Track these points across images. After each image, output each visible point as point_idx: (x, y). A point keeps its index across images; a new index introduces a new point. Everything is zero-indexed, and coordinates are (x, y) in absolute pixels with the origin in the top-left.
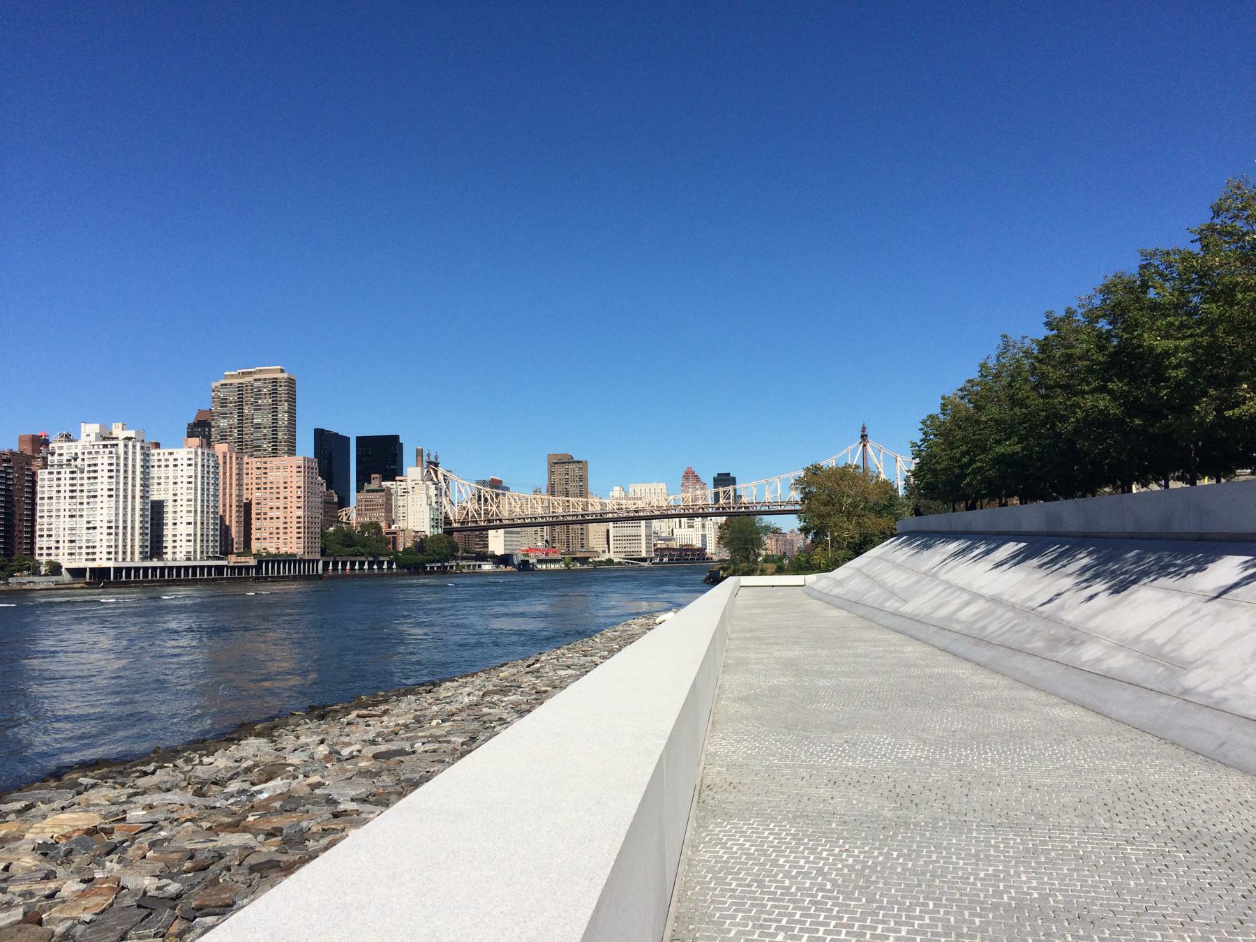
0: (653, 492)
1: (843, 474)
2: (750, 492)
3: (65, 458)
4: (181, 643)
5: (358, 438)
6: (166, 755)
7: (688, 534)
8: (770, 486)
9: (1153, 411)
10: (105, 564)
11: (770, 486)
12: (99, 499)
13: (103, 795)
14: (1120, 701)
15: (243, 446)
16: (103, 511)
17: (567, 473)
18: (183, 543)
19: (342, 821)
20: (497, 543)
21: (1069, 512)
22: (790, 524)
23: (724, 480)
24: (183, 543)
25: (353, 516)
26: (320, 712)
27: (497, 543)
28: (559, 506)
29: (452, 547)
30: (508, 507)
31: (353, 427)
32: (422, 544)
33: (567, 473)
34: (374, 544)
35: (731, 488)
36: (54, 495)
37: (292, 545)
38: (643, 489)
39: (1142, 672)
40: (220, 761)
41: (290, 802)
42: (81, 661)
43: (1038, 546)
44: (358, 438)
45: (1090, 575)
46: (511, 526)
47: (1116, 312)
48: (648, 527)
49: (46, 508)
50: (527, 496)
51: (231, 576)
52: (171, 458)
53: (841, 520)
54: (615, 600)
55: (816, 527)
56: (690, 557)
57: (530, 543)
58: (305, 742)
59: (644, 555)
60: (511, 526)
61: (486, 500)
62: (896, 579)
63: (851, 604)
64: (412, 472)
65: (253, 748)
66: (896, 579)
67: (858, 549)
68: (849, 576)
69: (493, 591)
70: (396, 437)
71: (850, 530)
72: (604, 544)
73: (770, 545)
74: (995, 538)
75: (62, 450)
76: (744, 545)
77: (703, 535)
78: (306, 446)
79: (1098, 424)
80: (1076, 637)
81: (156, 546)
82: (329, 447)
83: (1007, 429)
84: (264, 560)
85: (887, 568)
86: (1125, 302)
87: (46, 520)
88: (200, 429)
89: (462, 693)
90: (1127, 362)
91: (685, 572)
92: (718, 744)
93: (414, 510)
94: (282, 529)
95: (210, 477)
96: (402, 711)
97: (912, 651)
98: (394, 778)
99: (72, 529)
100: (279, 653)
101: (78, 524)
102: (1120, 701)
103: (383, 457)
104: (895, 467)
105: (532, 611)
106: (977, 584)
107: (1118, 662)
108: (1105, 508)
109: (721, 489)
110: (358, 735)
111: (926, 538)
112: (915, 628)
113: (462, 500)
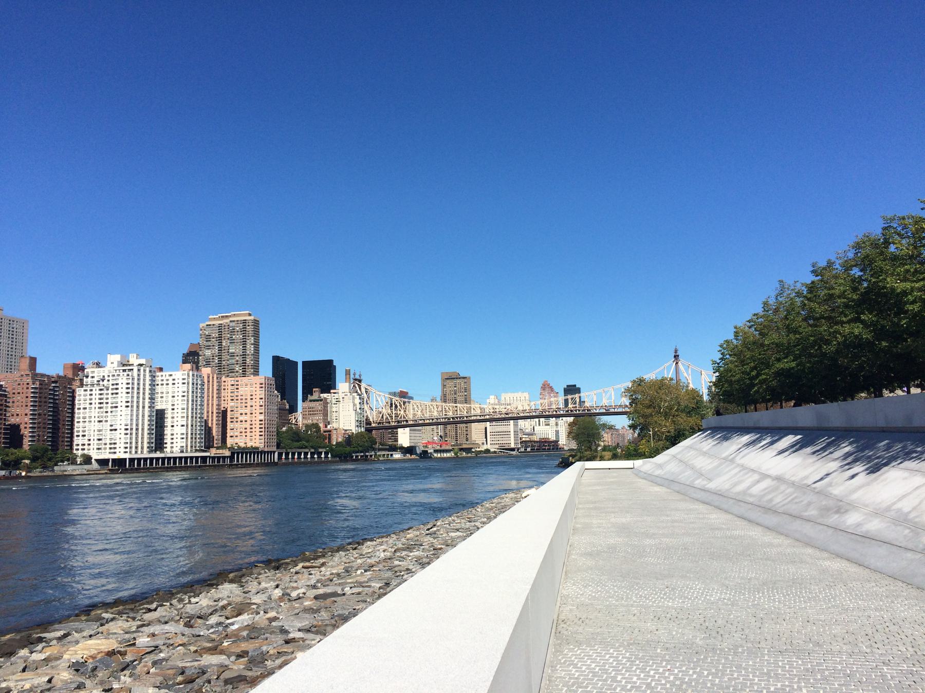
1: (661, 385)
2: (591, 398)
4: (176, 515)
6: (166, 595)
7: (545, 430)
8: (606, 393)
9: (896, 336)
11: (606, 393)
13: (119, 626)
14: (877, 556)
15: (222, 369)
16: (122, 417)
17: (456, 386)
18: (178, 442)
19: (292, 645)
20: (404, 438)
21: (833, 412)
22: (621, 422)
23: (571, 390)
24: (178, 442)
25: (300, 419)
26: (275, 564)
27: (404, 438)
29: (370, 442)
30: (412, 412)
31: (300, 355)
32: (349, 439)
33: (456, 386)
34: (315, 439)
37: (256, 441)
38: (512, 396)
39: (900, 534)
40: (203, 601)
41: (254, 632)
42: (102, 534)
43: (811, 438)
45: (851, 460)
46: (415, 425)
47: (866, 263)
50: (426, 403)
51: (212, 464)
53: (660, 420)
54: (492, 480)
55: (641, 425)
56: (547, 447)
57: (428, 438)
58: (265, 587)
62: (703, 463)
63: (668, 482)
64: (343, 386)
65: (227, 591)
66: (703, 463)
67: (674, 440)
68: (667, 461)
69: (400, 473)
71: (667, 427)
73: (607, 438)
74: (778, 432)
76: (588, 439)
77: (558, 431)
78: (266, 369)
79: (854, 345)
80: (841, 507)
81: (159, 443)
82: (283, 369)
83: (785, 350)
84: (238, 452)
85: (696, 455)
86: (872, 255)
88: (192, 357)
89: (378, 550)
90: (874, 299)
91: (544, 458)
92: (569, 589)
93: (344, 415)
94: (249, 430)
95: (198, 391)
96: (335, 564)
97: (716, 518)
98: (329, 614)
100: (247, 518)
101: (104, 427)
102: (877, 556)
103: (321, 376)
104: (700, 378)
105: (431, 489)
106: (763, 467)
107: (874, 526)
108: (862, 408)
110: (303, 581)
111: (725, 432)
112: (718, 500)
113: (378, 406)
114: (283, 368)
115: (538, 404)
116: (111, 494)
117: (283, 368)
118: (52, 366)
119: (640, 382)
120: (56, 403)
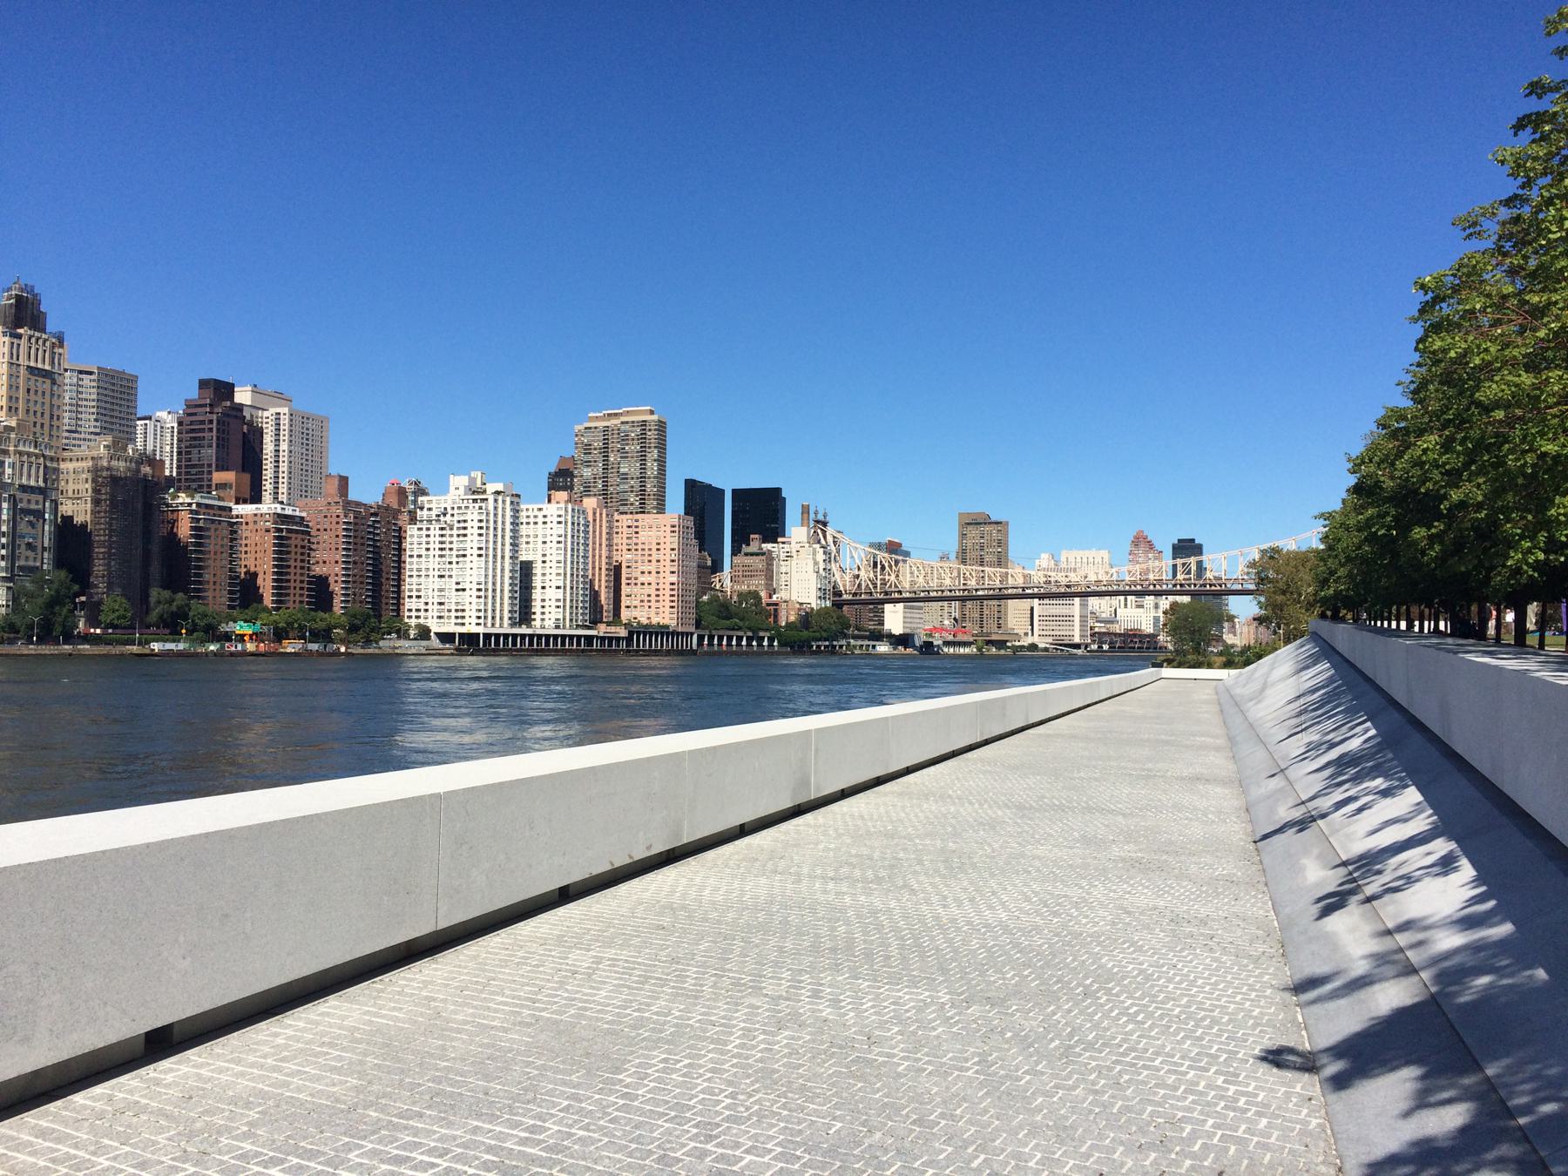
0: (1092, 563)
3: (434, 513)
5: (734, 491)
10: (474, 629)
12: (469, 538)
16: (473, 572)
17: (983, 536)
20: (894, 619)
23: (1187, 548)
24: (552, 611)
25: (725, 581)
27: (894, 619)
30: (908, 577)
31: (729, 478)
32: (807, 618)
33: (983, 536)
34: (750, 616)
35: (1193, 560)
36: (424, 552)
37: (665, 616)
44: (734, 491)
46: (914, 600)
48: (1084, 606)
49: (415, 567)
50: (931, 563)
52: (540, 514)
57: (934, 622)
59: (1077, 640)
60: (914, 600)
61: (883, 568)
64: (797, 532)
70: (778, 490)
75: (433, 503)
77: (1143, 617)
81: (524, 613)
84: (639, 631)
87: (415, 580)
88: (561, 479)
93: (799, 578)
94: (654, 599)
95: (580, 536)
99: (441, 590)
103: (762, 514)
109: (1179, 561)
113: (854, 566)
114: (701, 499)
115: (1127, 572)
117: (701, 499)
118: (368, 492)
119: (1272, 555)
120: (378, 543)
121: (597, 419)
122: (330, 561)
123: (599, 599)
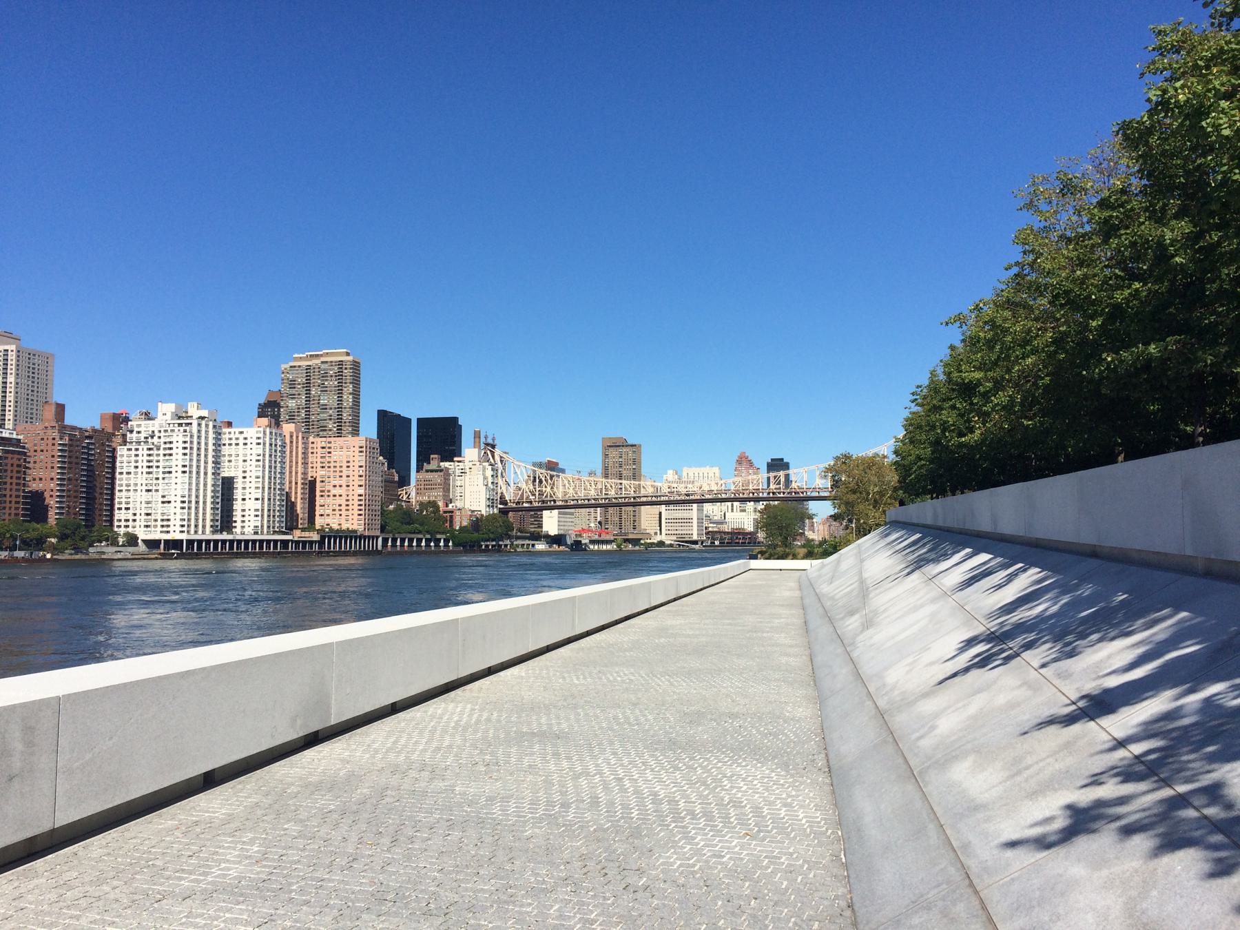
15: (310, 426)
16: (178, 486)
17: (621, 456)
18: (250, 519)
20: (551, 523)
23: (777, 465)
24: (250, 519)
25: (412, 494)
27: (551, 523)
28: (612, 489)
30: (562, 489)
31: (414, 409)
32: (477, 523)
33: (621, 456)
37: (353, 521)
46: (565, 507)
50: (583, 477)
57: (584, 524)
60: (565, 507)
64: (470, 453)
72: (652, 525)
75: (140, 427)
78: (369, 428)
81: (226, 520)
82: (391, 428)
84: (330, 536)
88: (270, 409)
93: (471, 490)
94: (344, 507)
95: (277, 453)
103: (442, 438)
113: (517, 481)
115: (732, 483)
116: (157, 595)
120: (91, 464)
121: (301, 359)
122: (45, 477)
123: (295, 508)
